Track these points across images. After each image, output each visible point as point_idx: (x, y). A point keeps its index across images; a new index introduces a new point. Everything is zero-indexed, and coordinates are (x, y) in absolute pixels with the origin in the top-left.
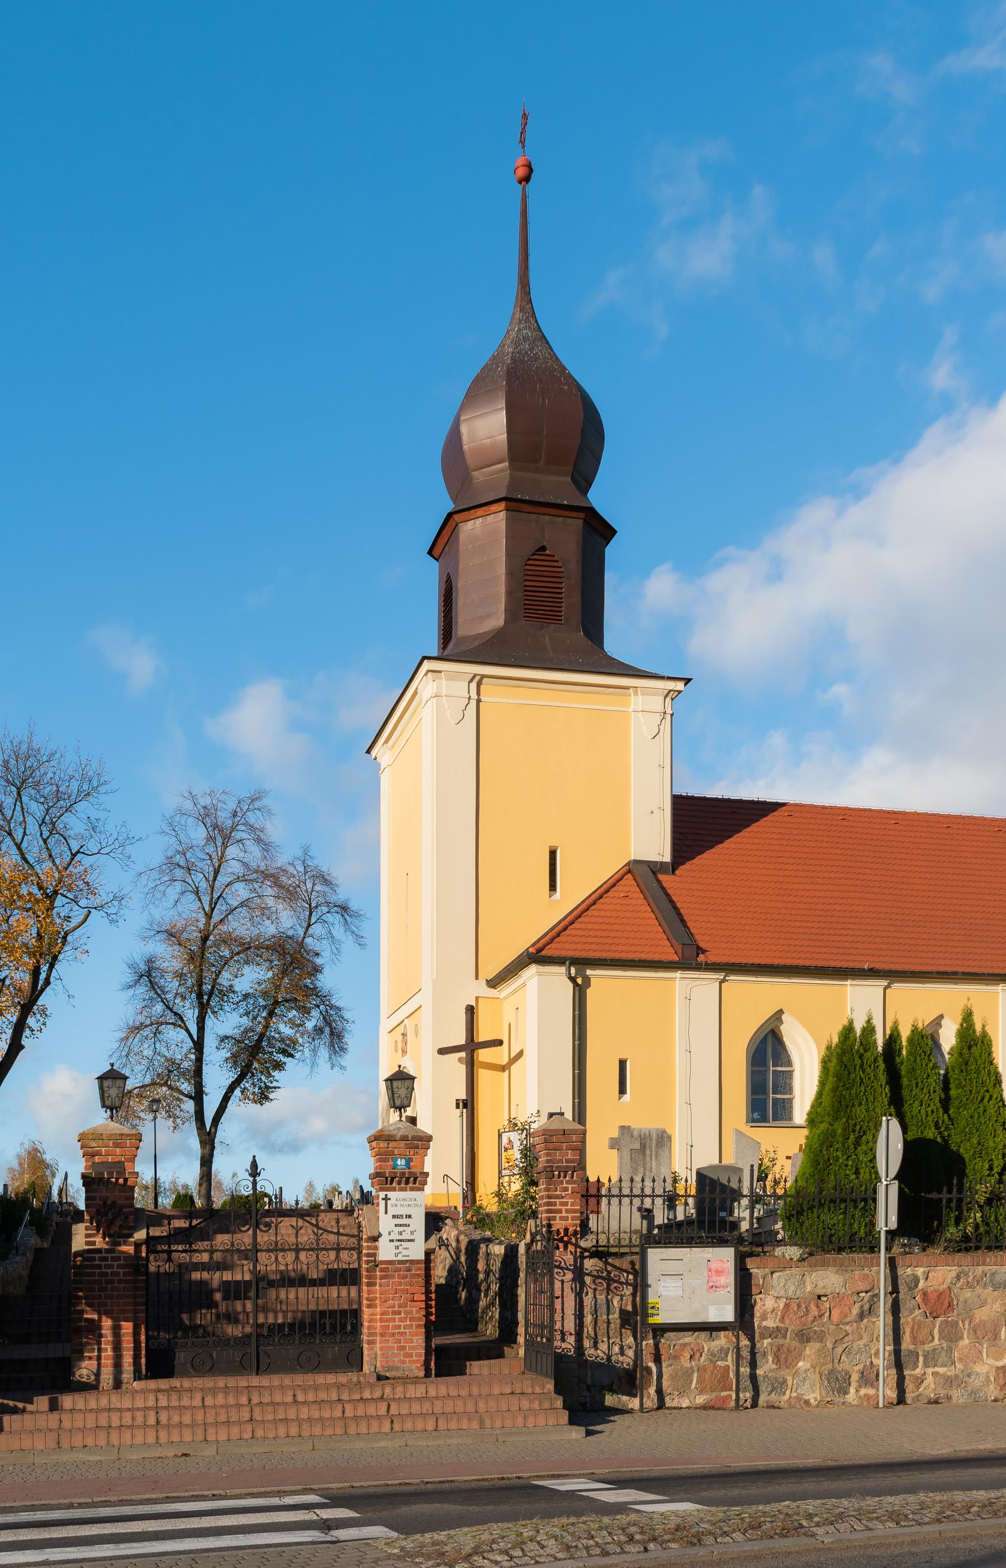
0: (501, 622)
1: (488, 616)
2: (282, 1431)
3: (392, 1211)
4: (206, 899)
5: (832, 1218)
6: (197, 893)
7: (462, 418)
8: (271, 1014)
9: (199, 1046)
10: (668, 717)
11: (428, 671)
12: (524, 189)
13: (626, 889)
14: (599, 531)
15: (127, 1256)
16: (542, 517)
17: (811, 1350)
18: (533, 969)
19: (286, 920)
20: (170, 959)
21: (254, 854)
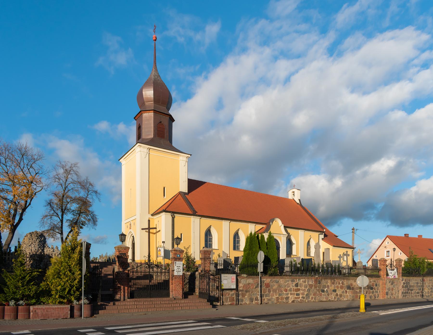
0: (152, 137)
2: (162, 309)
3: (177, 265)
4: (64, 187)
5: (250, 269)
6: (61, 185)
8: (79, 216)
9: (62, 221)
14: (172, 120)
15: (126, 273)
17: (247, 294)
18: (164, 213)
19: (82, 194)
20: (55, 200)
21: (75, 177)
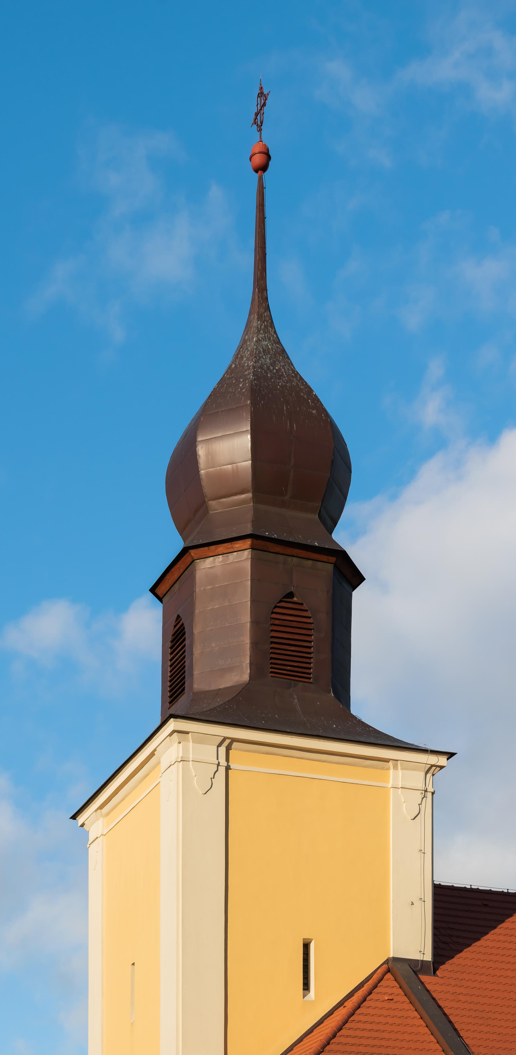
0: (246, 677)
1: (230, 669)
7: (199, 439)
10: (429, 795)
11: (174, 732)
12: (261, 180)
13: (389, 990)
14: (349, 575)
16: (289, 559)
